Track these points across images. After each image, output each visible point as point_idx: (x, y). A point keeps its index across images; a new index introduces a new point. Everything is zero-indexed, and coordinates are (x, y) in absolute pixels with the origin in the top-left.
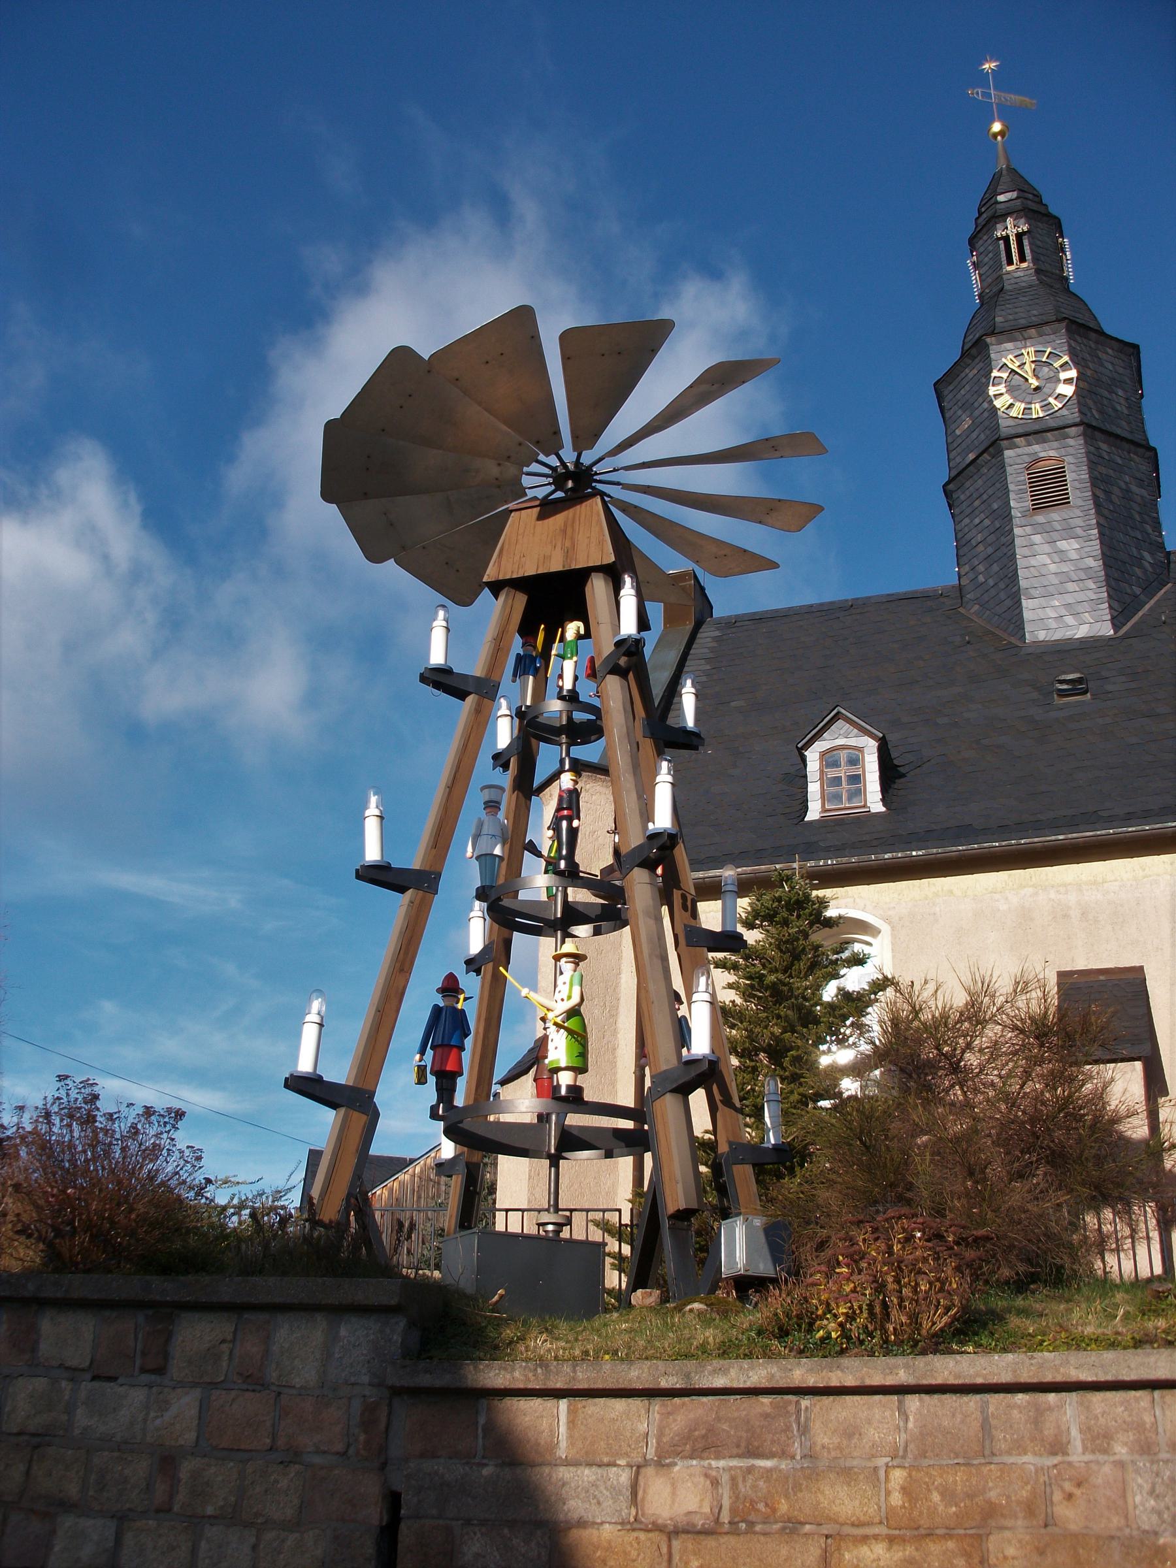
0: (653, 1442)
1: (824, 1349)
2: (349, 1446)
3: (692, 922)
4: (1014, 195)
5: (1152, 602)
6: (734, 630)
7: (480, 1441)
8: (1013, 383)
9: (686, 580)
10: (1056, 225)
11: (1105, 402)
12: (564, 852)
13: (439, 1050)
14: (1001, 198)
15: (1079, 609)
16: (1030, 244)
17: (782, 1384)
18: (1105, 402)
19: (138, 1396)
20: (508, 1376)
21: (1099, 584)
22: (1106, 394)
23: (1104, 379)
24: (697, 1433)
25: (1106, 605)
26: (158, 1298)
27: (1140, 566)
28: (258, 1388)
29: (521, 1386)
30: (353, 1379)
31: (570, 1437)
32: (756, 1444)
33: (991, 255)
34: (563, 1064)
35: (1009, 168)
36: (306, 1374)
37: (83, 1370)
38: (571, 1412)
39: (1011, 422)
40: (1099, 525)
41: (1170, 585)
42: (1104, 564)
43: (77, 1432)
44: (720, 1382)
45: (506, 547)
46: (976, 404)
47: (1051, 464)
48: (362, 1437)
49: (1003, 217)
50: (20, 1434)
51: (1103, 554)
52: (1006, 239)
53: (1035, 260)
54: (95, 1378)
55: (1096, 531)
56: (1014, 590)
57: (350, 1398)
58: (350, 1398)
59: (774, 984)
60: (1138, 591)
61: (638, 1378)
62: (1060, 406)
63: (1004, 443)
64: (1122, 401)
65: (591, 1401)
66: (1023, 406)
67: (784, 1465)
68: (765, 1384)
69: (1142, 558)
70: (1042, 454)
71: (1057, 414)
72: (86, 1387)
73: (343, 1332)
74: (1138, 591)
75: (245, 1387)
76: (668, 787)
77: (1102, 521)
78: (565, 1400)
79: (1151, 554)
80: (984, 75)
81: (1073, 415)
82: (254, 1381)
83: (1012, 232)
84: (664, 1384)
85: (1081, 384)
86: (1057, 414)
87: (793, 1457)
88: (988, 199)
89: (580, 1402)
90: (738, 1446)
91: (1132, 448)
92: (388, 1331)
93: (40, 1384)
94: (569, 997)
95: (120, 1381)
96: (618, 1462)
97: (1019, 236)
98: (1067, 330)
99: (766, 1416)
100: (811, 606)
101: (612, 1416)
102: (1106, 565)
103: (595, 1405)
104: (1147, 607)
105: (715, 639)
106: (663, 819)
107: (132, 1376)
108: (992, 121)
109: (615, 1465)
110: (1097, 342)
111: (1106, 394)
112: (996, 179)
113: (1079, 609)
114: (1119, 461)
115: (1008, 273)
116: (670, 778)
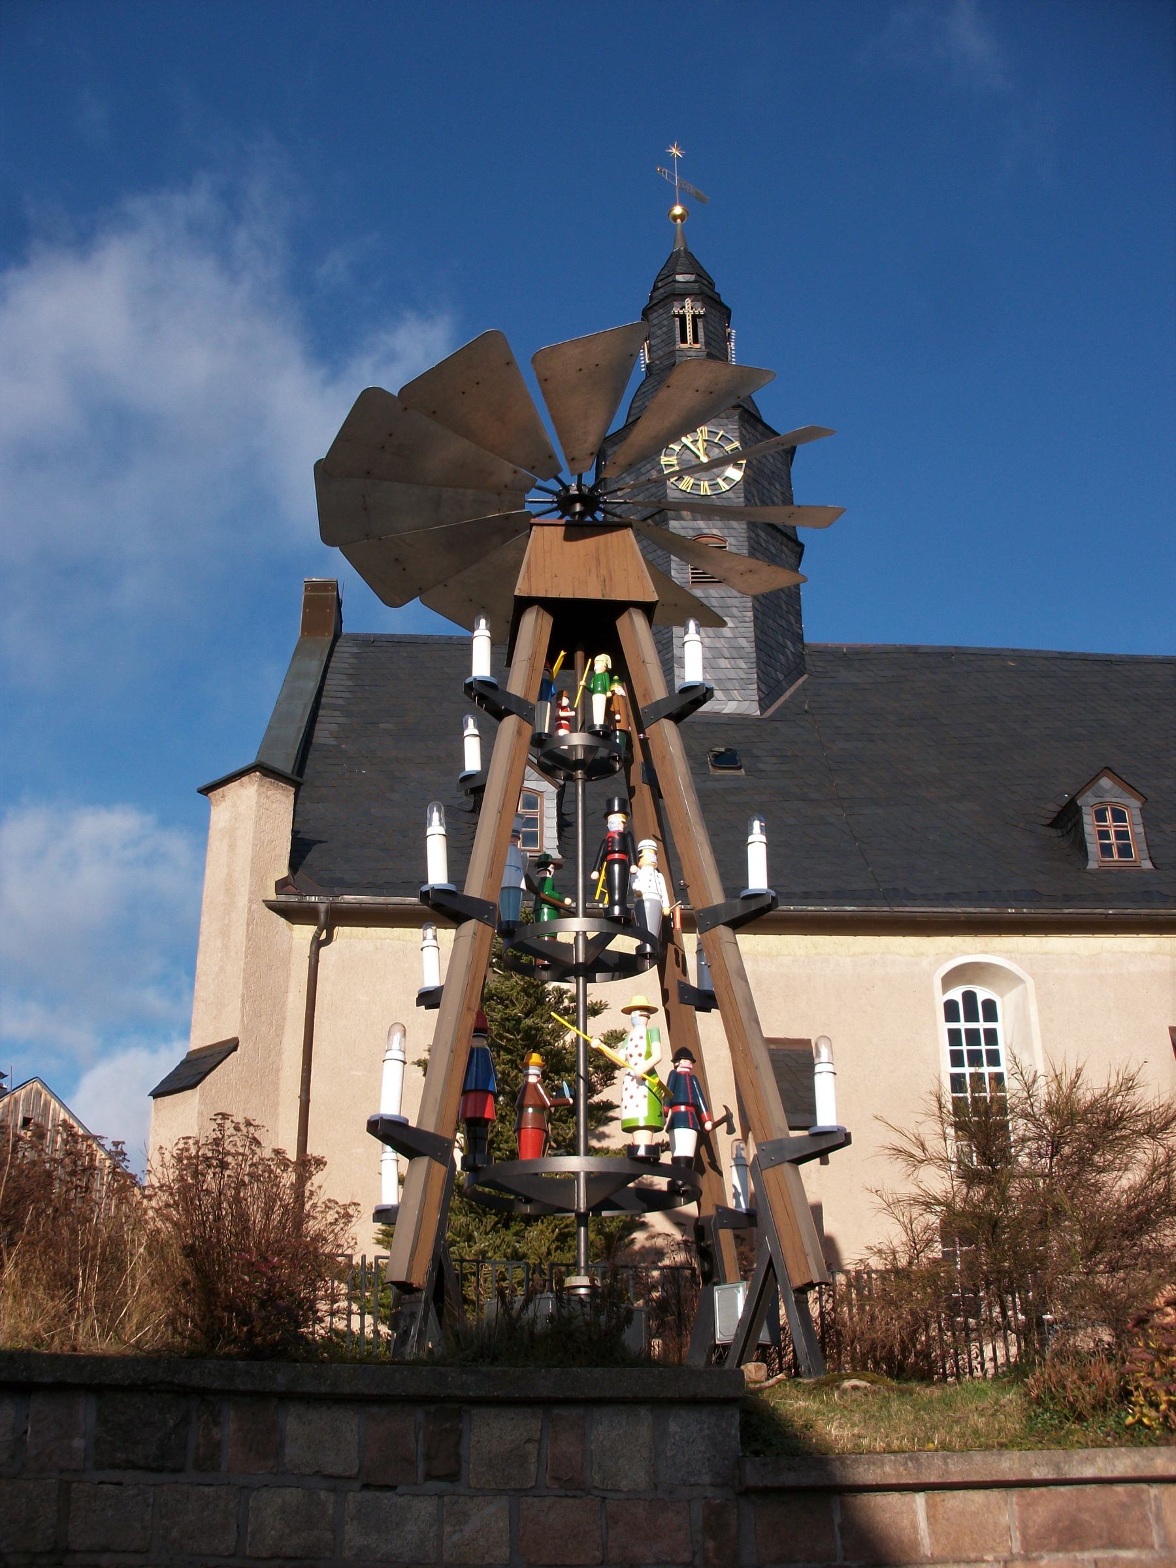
0: (1017, 1535)
1: (1136, 1436)
2: (694, 1554)
3: (683, 979)
4: (692, 278)
5: (792, 690)
6: (372, 649)
7: (839, 1542)
8: (684, 457)
9: (328, 591)
10: (726, 313)
11: (766, 492)
12: (617, 897)
13: (472, 1096)
14: (679, 278)
15: (730, 685)
16: (705, 328)
17: (1147, 1473)
18: (766, 492)
19: (424, 1508)
20: (879, 1471)
21: (750, 665)
22: (766, 484)
23: (766, 471)
24: (1060, 1525)
25: (755, 686)
26: (458, 1393)
27: (784, 654)
28: (578, 1493)
29: (894, 1481)
30: (692, 1480)
31: (933, 1533)
32: (1116, 1534)
33: (664, 329)
34: (642, 1123)
35: (686, 250)
36: (633, 1473)
37: (349, 1478)
38: (931, 1507)
39: (678, 494)
40: (754, 608)
41: (806, 676)
42: (756, 646)
43: (347, 1554)
44: (1089, 1472)
45: (533, 559)
46: (643, 470)
47: (714, 543)
48: (710, 1544)
49: (682, 296)
50: (274, 1557)
51: (756, 637)
52: (682, 318)
53: (707, 344)
54: (366, 1487)
55: (751, 614)
56: (667, 656)
57: (689, 1501)
58: (689, 1501)
59: (530, 1028)
60: (781, 677)
61: (1010, 1469)
62: (728, 488)
63: (671, 513)
64: (779, 495)
65: (949, 1494)
66: (692, 481)
67: (1144, 1555)
68: (1130, 1473)
69: (785, 647)
70: (706, 531)
71: (724, 495)
72: (355, 1498)
73: (673, 1427)
74: (781, 677)
75: (563, 1493)
76: (763, 848)
77: (757, 605)
78: (922, 1494)
79: (793, 644)
80: (670, 157)
81: (739, 500)
82: (572, 1485)
83: (689, 312)
84: (1036, 1474)
85: (748, 472)
86: (724, 495)
87: (1152, 1547)
88: (667, 274)
89: (939, 1496)
90: (1101, 1537)
91: (785, 540)
92: (724, 1425)
93: (293, 1496)
94: (649, 1055)
95: (399, 1490)
96: (986, 1558)
97: (694, 317)
98: (740, 417)
99: (1123, 1505)
100: (451, 638)
101: (973, 1509)
102: (758, 649)
103: (954, 1498)
104: (788, 694)
105: (354, 655)
106: (758, 879)
107: (416, 1484)
108: (675, 204)
109: (983, 1561)
110: (762, 435)
111: (766, 484)
112: (673, 259)
113: (730, 685)
114: (774, 551)
115: (682, 350)
116: (763, 838)
